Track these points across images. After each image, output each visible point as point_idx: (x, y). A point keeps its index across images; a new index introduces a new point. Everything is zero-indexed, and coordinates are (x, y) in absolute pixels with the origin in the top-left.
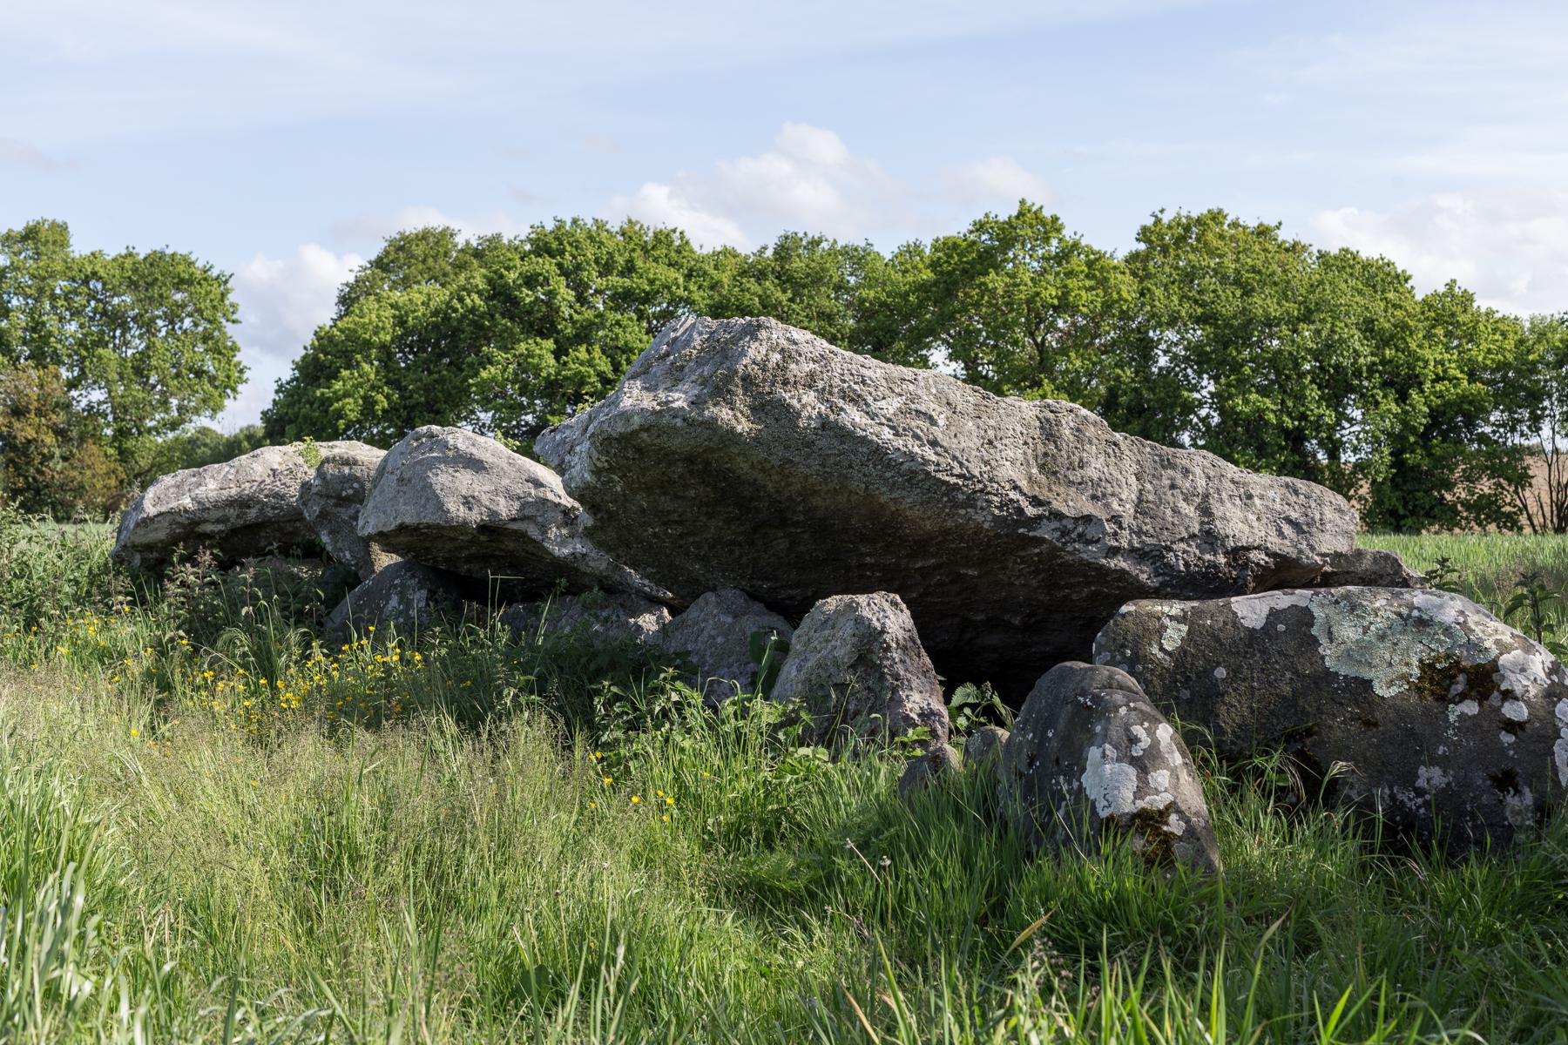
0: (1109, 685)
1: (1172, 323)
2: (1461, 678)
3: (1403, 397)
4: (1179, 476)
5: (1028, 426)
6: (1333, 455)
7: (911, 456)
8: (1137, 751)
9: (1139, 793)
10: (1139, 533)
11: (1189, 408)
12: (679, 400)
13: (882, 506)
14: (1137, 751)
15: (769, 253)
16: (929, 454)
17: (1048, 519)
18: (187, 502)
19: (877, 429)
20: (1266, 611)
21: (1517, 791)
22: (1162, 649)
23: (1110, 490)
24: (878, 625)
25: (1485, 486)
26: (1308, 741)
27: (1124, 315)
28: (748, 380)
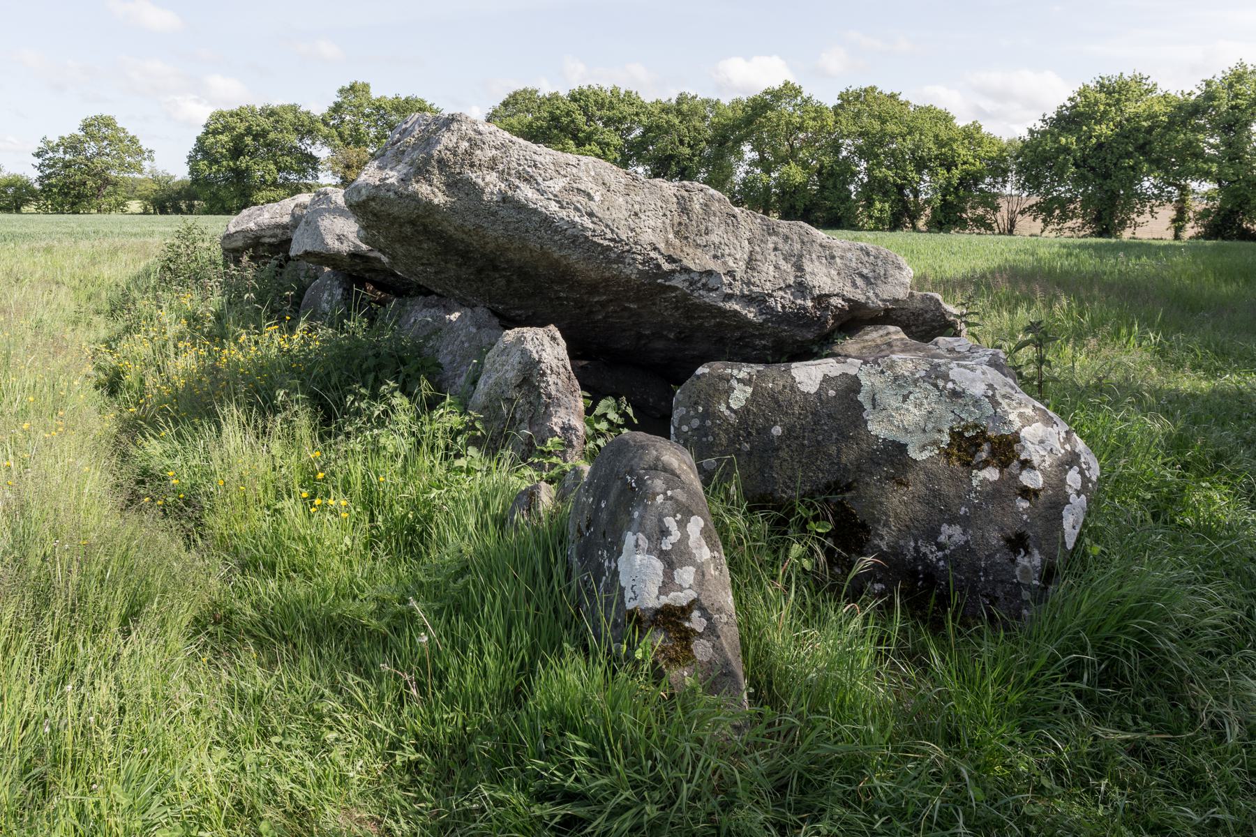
0: (658, 467)
1: (848, 137)
2: (986, 447)
3: (949, 170)
4: (780, 241)
5: (667, 202)
6: (916, 196)
7: (573, 224)
8: (666, 545)
9: (664, 589)
10: (749, 283)
11: (854, 174)
12: (393, 177)
13: (557, 260)
14: (666, 545)
15: (674, 102)
16: (587, 222)
17: (680, 272)
18: (252, 225)
19: (545, 203)
20: (820, 378)
21: (1027, 553)
22: (729, 407)
23: (727, 251)
24: (536, 356)
25: (980, 211)
26: (848, 495)
27: (829, 133)
28: (442, 163)
